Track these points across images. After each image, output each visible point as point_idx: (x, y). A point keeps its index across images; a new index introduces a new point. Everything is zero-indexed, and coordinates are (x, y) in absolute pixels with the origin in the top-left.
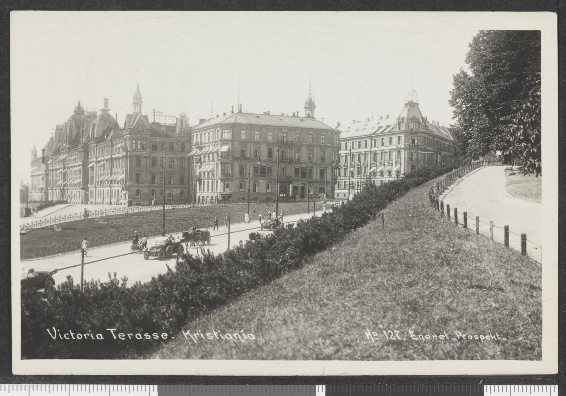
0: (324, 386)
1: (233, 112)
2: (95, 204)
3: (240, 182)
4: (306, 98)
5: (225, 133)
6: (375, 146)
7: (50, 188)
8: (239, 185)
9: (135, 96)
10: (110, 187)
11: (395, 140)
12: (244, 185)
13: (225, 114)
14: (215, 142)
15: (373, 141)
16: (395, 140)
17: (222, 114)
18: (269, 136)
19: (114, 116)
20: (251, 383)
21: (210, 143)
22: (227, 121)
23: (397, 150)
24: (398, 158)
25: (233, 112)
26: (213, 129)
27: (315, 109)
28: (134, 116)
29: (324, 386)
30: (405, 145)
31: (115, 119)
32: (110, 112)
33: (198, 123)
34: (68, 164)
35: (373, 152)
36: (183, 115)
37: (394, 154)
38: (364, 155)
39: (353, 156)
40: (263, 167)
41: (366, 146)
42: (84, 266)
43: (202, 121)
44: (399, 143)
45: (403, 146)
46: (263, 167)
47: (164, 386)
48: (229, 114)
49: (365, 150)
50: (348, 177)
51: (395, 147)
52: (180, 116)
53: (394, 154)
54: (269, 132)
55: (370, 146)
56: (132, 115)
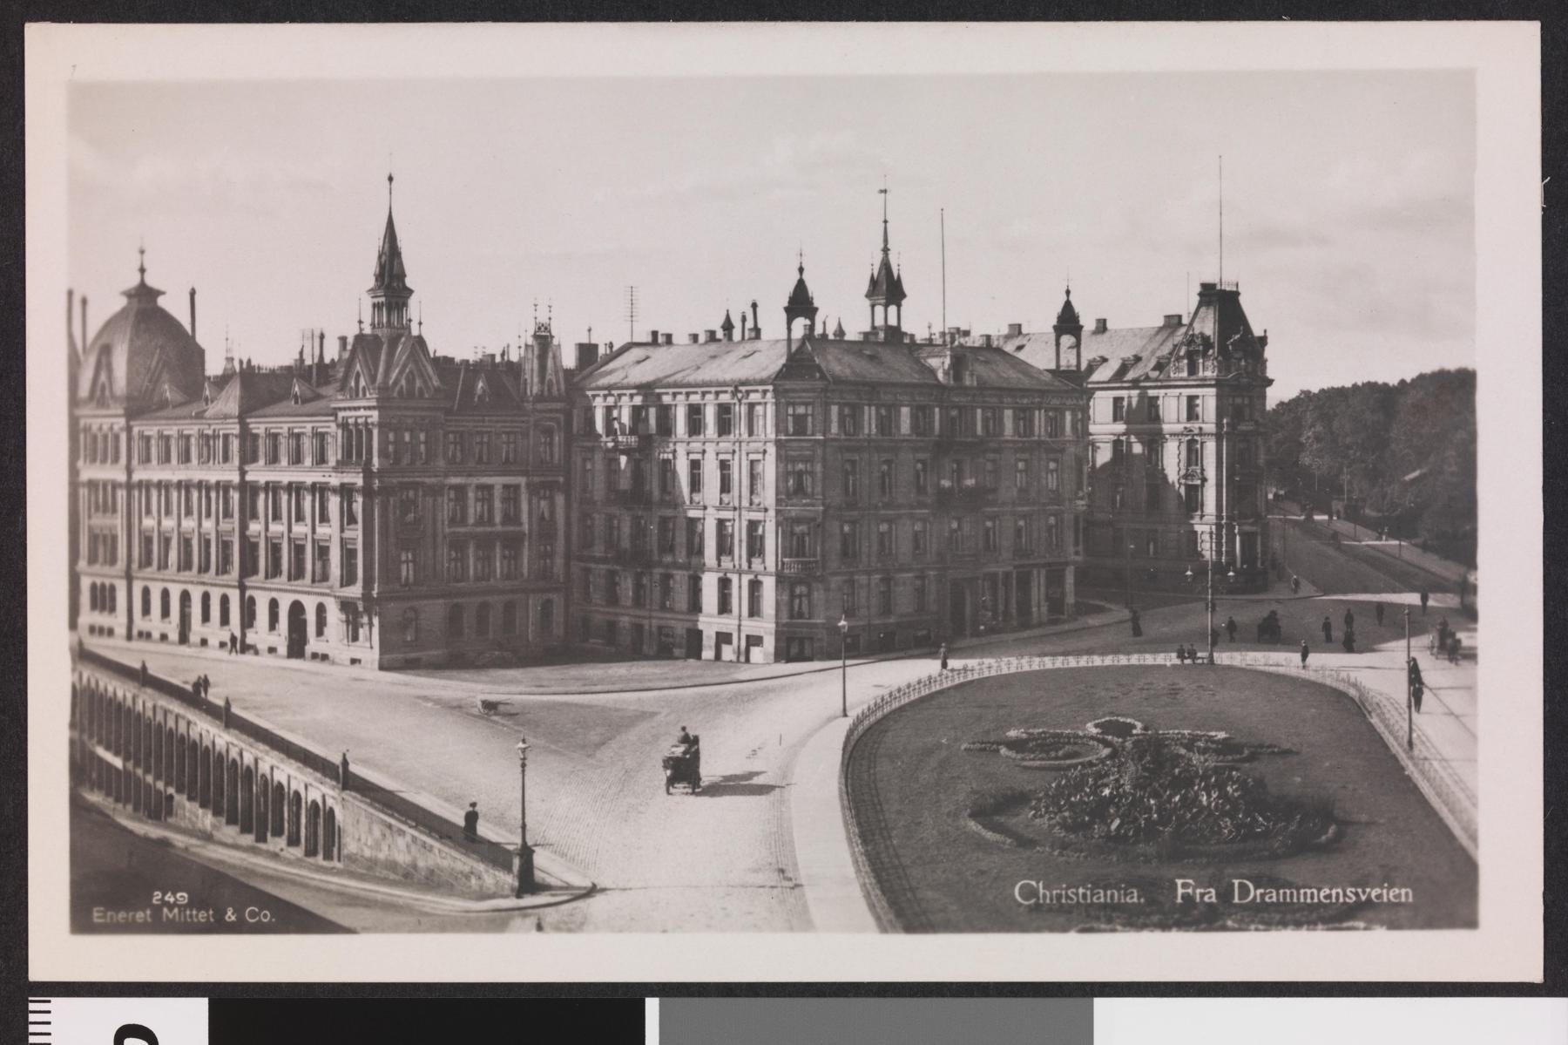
0: (32, 1007)
10: (242, 588)
29: (32, 1007)
32: (162, 302)
47: (665, 999)
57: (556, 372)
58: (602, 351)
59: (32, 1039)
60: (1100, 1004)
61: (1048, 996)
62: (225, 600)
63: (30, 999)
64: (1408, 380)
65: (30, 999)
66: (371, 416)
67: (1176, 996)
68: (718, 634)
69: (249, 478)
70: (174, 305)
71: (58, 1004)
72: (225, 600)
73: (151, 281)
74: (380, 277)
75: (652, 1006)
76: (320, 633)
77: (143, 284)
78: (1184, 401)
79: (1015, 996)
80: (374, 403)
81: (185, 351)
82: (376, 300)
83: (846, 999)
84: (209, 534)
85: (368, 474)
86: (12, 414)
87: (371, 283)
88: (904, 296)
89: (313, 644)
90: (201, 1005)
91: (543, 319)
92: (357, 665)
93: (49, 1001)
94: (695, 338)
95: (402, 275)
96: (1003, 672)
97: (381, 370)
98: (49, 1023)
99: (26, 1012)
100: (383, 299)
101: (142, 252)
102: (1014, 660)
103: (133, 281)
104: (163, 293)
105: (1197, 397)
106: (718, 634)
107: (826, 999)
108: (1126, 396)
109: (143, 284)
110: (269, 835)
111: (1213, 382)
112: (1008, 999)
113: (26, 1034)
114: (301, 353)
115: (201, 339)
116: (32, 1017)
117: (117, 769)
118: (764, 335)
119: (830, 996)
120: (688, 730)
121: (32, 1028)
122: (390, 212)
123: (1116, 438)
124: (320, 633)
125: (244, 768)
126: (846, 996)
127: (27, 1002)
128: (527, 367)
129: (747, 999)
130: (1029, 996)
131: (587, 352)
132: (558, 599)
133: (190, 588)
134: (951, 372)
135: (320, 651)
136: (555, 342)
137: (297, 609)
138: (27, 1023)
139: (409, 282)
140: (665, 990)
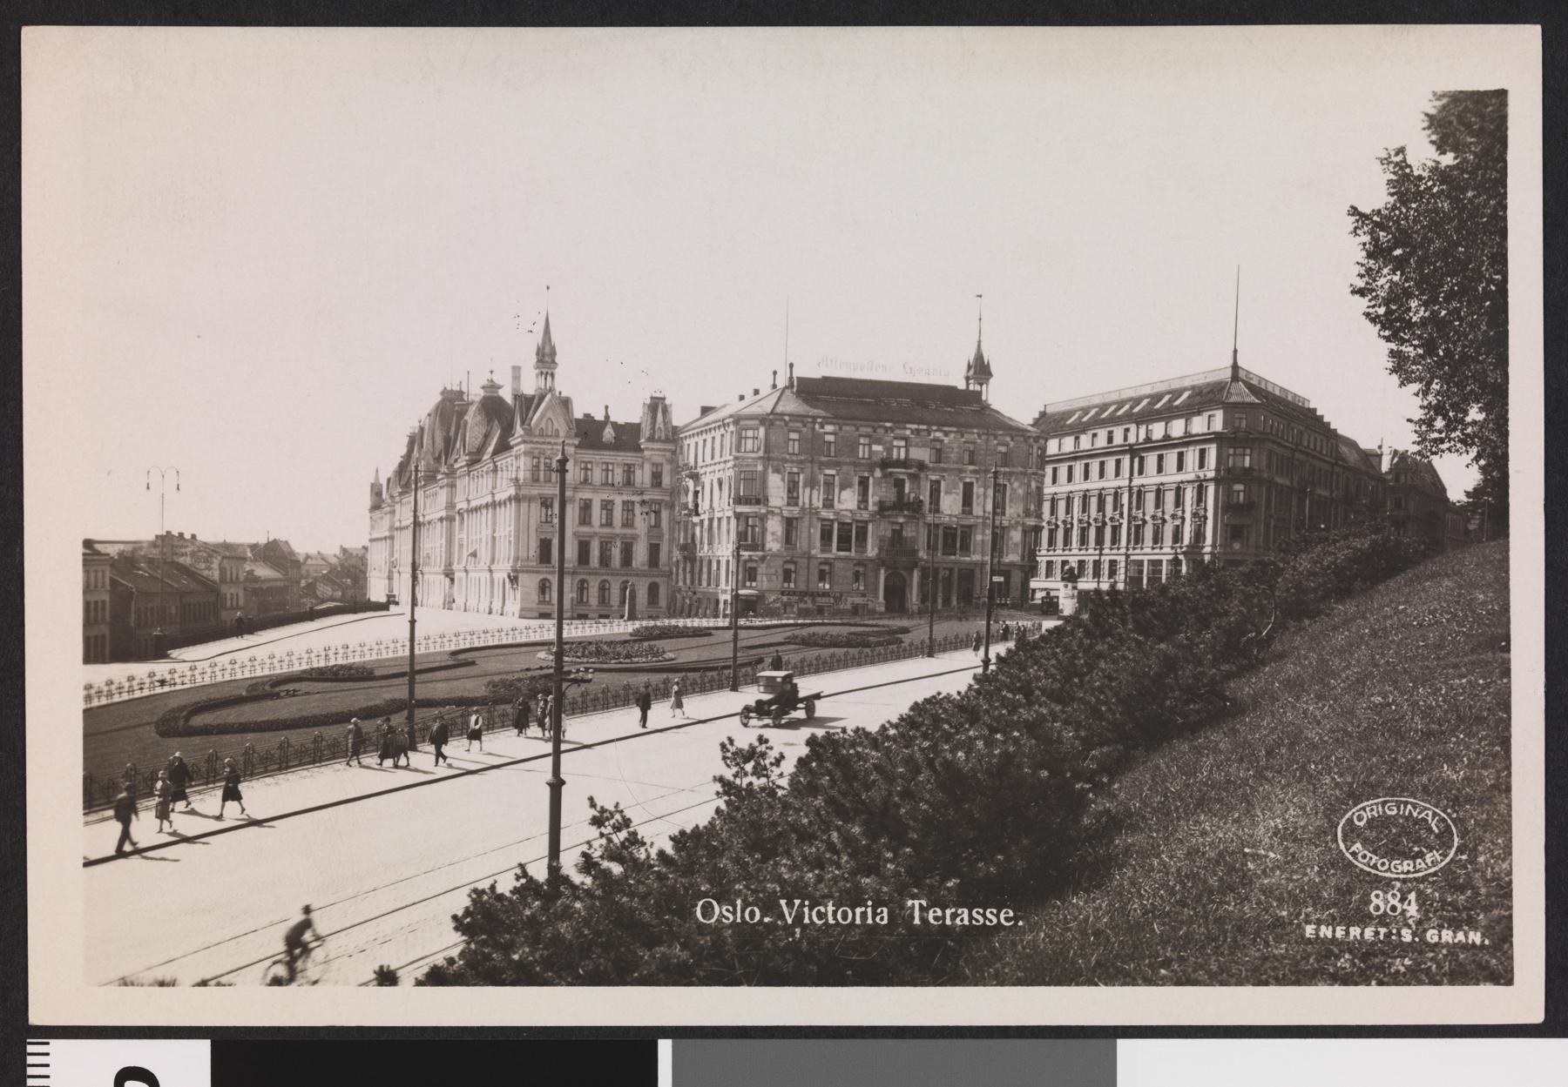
0: (30, 1049)
1: (774, 386)
2: (465, 610)
3: (786, 562)
4: (971, 355)
5: (746, 438)
6: (1141, 472)
7: (461, 567)
8: (780, 572)
9: (538, 349)
11: (1191, 456)
12: (830, 573)
13: (756, 392)
14: (707, 466)
15: (1136, 461)
16: (1191, 456)
17: (752, 392)
18: (861, 447)
20: (738, 1037)
21: (707, 466)
22: (755, 410)
23: (1197, 484)
24: (1084, 511)
25: (774, 386)
26: (722, 429)
27: (991, 380)
28: (537, 398)
29: (30, 1049)
33: (698, 414)
34: (424, 516)
35: (1135, 489)
37: (1189, 495)
38: (409, 533)
39: (1139, 495)
40: (846, 527)
41: (1117, 474)
42: (563, 756)
43: (706, 410)
44: (1202, 466)
45: (1211, 474)
46: (846, 527)
47: (678, 1040)
48: (765, 389)
49: (1085, 486)
50: (1123, 551)
51: (1191, 477)
52: (652, 398)
53: (1189, 495)
54: (860, 436)
55: (1127, 475)
56: (534, 396)
57: (666, 429)
59: (30, 1082)
60: (1123, 1045)
61: (1069, 1037)
63: (28, 1040)
64: (688, 831)
65: (28, 1040)
67: (1201, 1037)
71: (56, 1046)
75: (665, 1047)
78: (1083, 466)
79: (1037, 1038)
83: (863, 1041)
86: (9, 443)
88: (990, 375)
90: (204, 1047)
93: (48, 1043)
98: (48, 1065)
99: (25, 1054)
107: (842, 1041)
112: (1029, 1041)
113: (25, 1077)
114: (724, 406)
116: (30, 1060)
119: (847, 1038)
120: (599, 803)
121: (30, 1071)
122: (979, 346)
126: (863, 1038)
127: (25, 1044)
128: (643, 426)
129: (762, 1040)
130: (1050, 1037)
134: (946, 429)
138: (25, 1065)
140: (675, 1033)
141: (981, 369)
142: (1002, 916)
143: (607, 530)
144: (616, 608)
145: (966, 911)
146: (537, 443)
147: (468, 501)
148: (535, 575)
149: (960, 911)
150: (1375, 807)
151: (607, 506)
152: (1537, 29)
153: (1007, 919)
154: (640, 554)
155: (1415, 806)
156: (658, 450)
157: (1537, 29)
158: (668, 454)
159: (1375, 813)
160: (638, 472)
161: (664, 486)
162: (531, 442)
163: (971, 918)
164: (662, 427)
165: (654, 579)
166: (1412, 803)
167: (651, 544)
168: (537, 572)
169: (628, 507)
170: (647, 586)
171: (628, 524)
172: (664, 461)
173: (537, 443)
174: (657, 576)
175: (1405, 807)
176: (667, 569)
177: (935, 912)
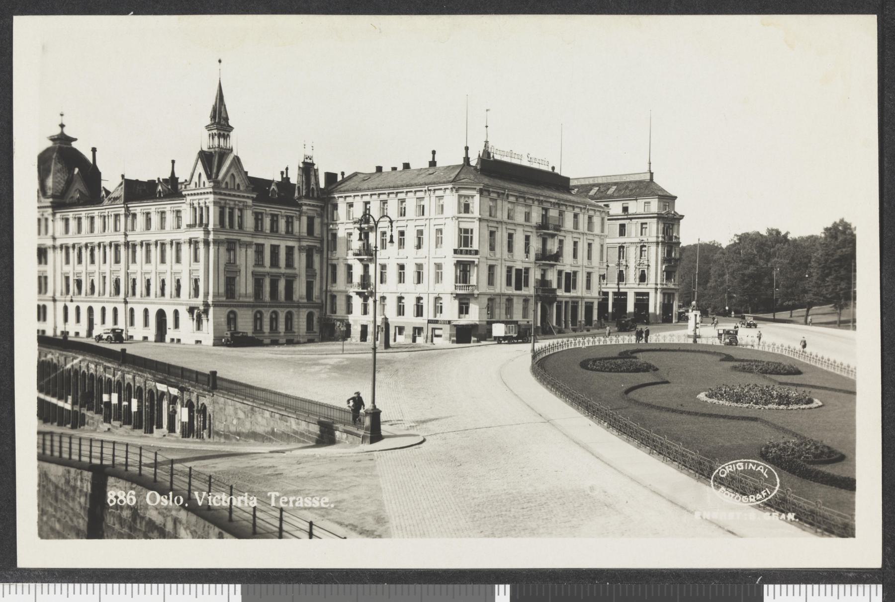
10: (126, 302)
19: (89, 156)
30: (658, 237)
31: (91, 162)
36: (308, 161)
49: (622, 240)
51: (637, 240)
58: (339, 178)
62: (115, 310)
66: (208, 199)
68: (415, 329)
69: (129, 239)
70: (82, 147)
72: (115, 310)
73: (68, 132)
74: (213, 117)
76: (177, 326)
77: (62, 133)
80: (211, 190)
81: (91, 174)
82: (210, 132)
84: (105, 273)
85: (207, 232)
87: (208, 121)
89: (171, 334)
91: (309, 154)
92: (199, 344)
94: (394, 169)
95: (227, 119)
96: (660, 342)
97: (215, 171)
100: (215, 131)
101: (62, 126)
102: (627, 337)
103: (57, 131)
104: (75, 140)
105: (646, 223)
106: (415, 329)
108: (648, 222)
109: (62, 133)
110: (112, 420)
111: (656, 215)
115: (100, 165)
117: (67, 410)
118: (438, 165)
123: (620, 245)
124: (177, 326)
125: (159, 394)
131: (331, 177)
132: (316, 313)
133: (93, 305)
135: (176, 338)
136: (315, 167)
137: (161, 314)
139: (231, 123)
141: (553, 168)
142: (322, 501)
143: (274, 270)
144: (282, 334)
145: (301, 498)
146: (225, 194)
147: (54, 238)
148: (225, 309)
149: (297, 499)
150: (730, 466)
151: (275, 249)
152: (875, 16)
153: (326, 503)
154: (300, 289)
155: (754, 464)
156: (313, 206)
157: (875, 16)
158: (318, 209)
159: (731, 469)
160: (296, 224)
161: (315, 235)
162: (220, 194)
163: (304, 502)
164: (315, 187)
165: (312, 310)
166: (752, 463)
167: (227, 277)
168: (226, 306)
169: (290, 250)
170: (306, 314)
171: (289, 264)
172: (315, 215)
173: (225, 194)
174: (277, 307)
175: (748, 465)
176: (319, 301)
177: (283, 499)
